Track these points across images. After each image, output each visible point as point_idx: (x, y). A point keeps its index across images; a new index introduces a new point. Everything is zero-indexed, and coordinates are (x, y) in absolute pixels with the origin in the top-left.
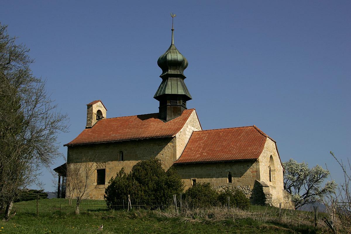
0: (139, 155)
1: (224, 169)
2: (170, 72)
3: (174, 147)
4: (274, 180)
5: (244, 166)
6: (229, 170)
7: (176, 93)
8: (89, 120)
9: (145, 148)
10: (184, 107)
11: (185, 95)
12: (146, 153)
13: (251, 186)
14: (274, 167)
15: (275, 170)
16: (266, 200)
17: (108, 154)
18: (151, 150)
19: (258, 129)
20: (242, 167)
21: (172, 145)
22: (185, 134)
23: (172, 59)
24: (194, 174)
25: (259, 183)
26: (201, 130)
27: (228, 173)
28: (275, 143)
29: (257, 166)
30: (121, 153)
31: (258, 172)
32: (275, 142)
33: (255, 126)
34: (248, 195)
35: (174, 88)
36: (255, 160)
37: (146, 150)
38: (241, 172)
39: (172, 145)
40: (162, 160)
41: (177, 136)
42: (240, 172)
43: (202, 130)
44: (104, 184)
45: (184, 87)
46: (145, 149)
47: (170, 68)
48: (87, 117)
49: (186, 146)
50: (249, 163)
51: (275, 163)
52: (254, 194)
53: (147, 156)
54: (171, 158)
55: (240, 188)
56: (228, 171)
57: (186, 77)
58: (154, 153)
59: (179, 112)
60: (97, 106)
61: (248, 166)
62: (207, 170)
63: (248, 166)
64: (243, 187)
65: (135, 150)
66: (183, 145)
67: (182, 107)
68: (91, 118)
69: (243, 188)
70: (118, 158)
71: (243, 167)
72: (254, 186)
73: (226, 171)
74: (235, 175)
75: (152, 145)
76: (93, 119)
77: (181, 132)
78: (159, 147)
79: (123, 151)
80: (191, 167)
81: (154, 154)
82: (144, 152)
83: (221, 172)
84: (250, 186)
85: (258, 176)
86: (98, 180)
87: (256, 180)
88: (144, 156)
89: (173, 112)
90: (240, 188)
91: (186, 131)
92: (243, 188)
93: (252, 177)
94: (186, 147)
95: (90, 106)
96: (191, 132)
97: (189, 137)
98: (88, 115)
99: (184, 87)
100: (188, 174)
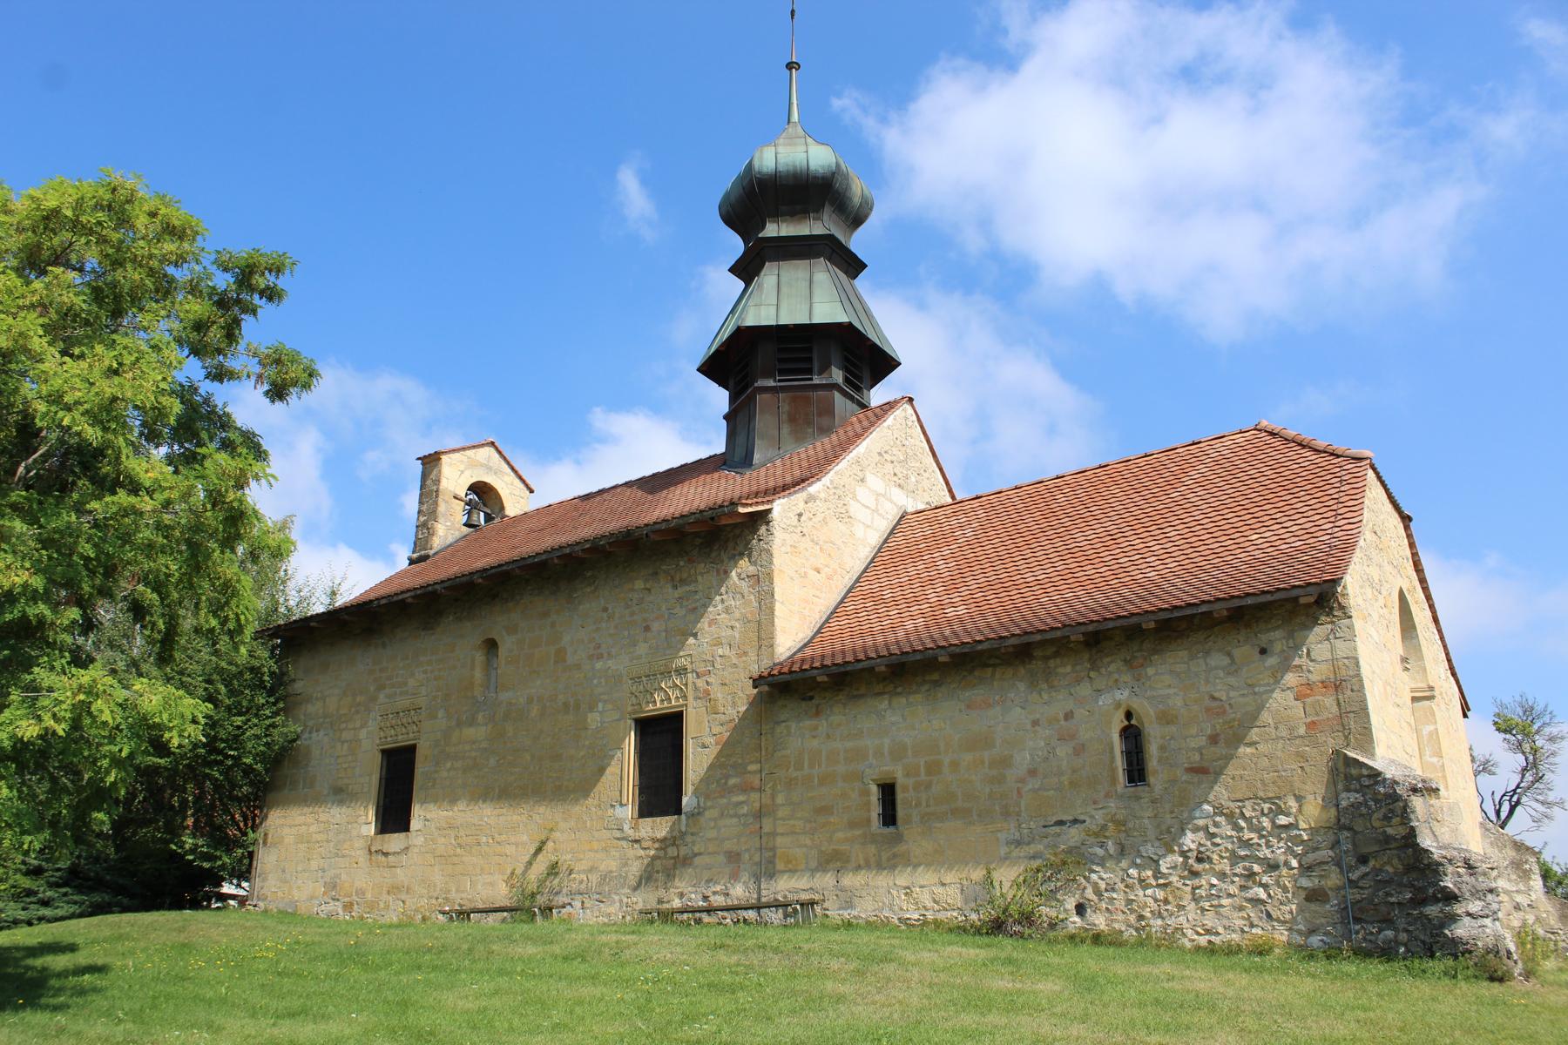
1: (1085, 690)
2: (771, 230)
3: (763, 583)
4: (1435, 760)
5: (1229, 654)
6: (1122, 695)
7: (802, 319)
10: (852, 398)
11: (850, 324)
13: (1299, 798)
14: (1425, 670)
15: (1431, 688)
16: (1459, 909)
18: (632, 614)
19: (1291, 433)
20: (1218, 660)
21: (752, 569)
22: (845, 517)
23: (780, 168)
24: (887, 741)
25: (1375, 775)
26: (950, 500)
27: (1120, 715)
28: (1407, 528)
29: (1338, 643)
31: (1345, 686)
32: (1406, 519)
33: (1264, 423)
34: (1284, 871)
35: (798, 297)
36: (1316, 601)
38: (1213, 698)
39: (752, 569)
41: (775, 514)
42: (1207, 702)
43: (953, 497)
44: (407, 829)
45: (851, 300)
47: (785, 214)
49: (852, 587)
50: (1269, 630)
51: (1424, 649)
52: (1338, 864)
54: (745, 654)
55: (1216, 825)
56: (1118, 705)
58: (647, 629)
59: (825, 421)
60: (473, 464)
61: (1263, 651)
62: (969, 707)
63: (1263, 651)
64: (1243, 815)
66: (829, 578)
67: (837, 395)
69: (1242, 823)
71: (1227, 661)
72: (1332, 800)
73: (1105, 701)
74: (1173, 729)
75: (639, 584)
76: (441, 520)
77: (811, 499)
78: (678, 593)
80: (862, 696)
83: (1069, 716)
84: (1292, 803)
85: (1352, 716)
87: (1337, 752)
88: (600, 657)
89: (792, 419)
90: (1216, 825)
91: (854, 498)
92: (1242, 823)
93: (1302, 731)
94: (849, 591)
95: (431, 462)
96: (892, 516)
97: (875, 539)
98: (421, 503)
99: (851, 300)
100: (849, 744)
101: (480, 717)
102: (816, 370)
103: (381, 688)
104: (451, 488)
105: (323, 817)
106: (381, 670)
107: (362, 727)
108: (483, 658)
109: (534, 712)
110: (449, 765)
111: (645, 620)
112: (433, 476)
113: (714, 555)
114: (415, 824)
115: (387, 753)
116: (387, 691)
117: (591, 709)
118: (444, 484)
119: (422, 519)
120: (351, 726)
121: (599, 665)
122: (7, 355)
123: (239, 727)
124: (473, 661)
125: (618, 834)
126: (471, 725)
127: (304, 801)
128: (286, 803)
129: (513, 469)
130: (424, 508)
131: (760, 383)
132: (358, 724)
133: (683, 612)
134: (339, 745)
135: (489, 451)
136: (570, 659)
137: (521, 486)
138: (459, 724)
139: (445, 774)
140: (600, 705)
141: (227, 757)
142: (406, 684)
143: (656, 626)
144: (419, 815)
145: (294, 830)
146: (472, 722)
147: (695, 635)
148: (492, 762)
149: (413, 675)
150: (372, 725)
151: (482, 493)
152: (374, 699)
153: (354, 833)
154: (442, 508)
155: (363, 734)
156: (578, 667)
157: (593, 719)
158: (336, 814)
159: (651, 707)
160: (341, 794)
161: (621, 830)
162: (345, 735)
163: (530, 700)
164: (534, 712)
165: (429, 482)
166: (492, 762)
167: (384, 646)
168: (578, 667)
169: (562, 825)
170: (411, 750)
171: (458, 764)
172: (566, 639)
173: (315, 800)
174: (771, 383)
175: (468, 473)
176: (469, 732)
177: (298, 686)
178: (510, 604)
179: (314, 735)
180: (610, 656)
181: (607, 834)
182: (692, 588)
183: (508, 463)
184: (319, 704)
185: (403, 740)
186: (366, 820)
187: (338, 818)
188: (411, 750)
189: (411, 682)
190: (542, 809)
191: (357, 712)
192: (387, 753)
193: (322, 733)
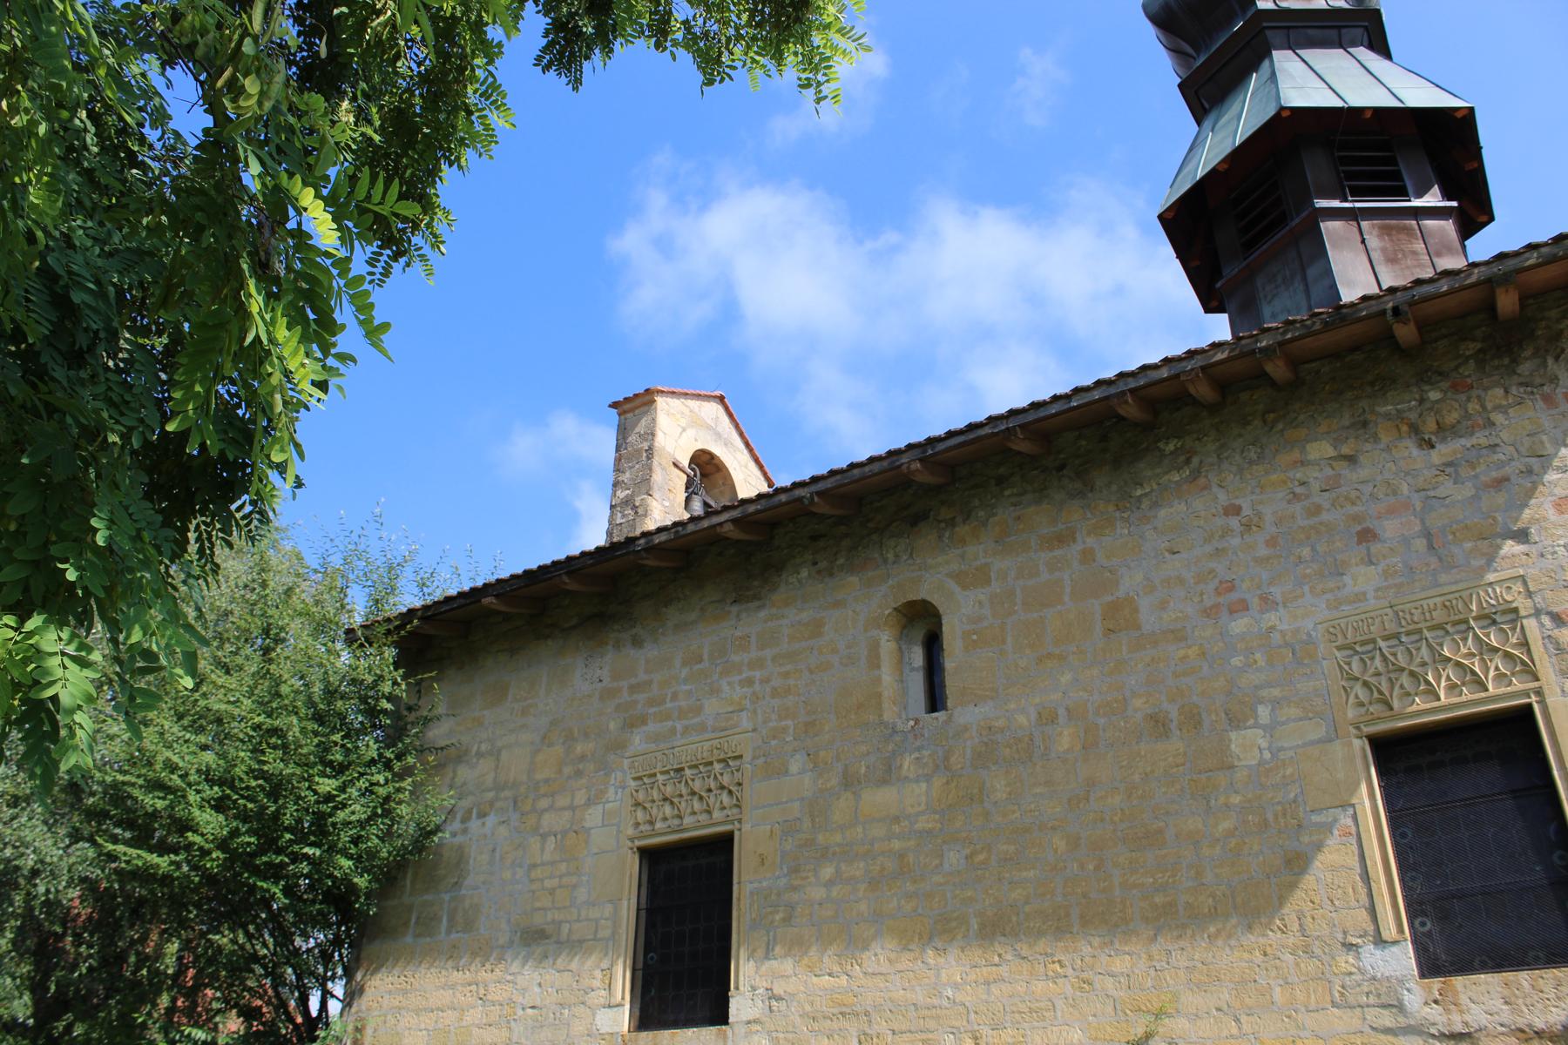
0: (1163, 605)
8: (628, 502)
9: (1237, 510)
12: (1260, 561)
17: (758, 664)
18: (1317, 510)
30: (919, 634)
37: (1247, 526)
40: (1537, 613)
46: (1234, 522)
48: (616, 485)
53: (1277, 592)
57: (644, 1034)
65: (1087, 556)
68: (644, 484)
70: (878, 680)
75: (1321, 449)
76: (656, 495)
78: (1436, 456)
79: (935, 599)
81: (1375, 548)
82: (1219, 552)
86: (1415, 908)
88: (1240, 607)
95: (633, 408)
98: (618, 469)
101: (907, 764)
102: (1410, 190)
103: (632, 723)
104: (670, 449)
105: (497, 993)
106: (633, 689)
107: (589, 803)
108: (892, 645)
109: (1065, 738)
110: (828, 872)
111: (1356, 518)
112: (641, 427)
113: (1525, 368)
114: (740, 1006)
115: (652, 857)
116: (651, 727)
117: (1236, 721)
118: (661, 440)
119: (621, 494)
120: (562, 801)
121: (1239, 625)
122: (5, 873)
123: (329, 798)
124: (874, 647)
125: (1387, 1019)
126: (884, 782)
127: (453, 954)
128: (413, 957)
129: (747, 445)
130: (626, 477)
131: (1322, 203)
132: (580, 798)
133: (1467, 491)
134: (534, 843)
135: (713, 410)
136: (1149, 619)
137: (758, 473)
138: (850, 782)
139: (818, 893)
140: (1264, 712)
141: (296, 858)
142: (698, 710)
143: (1390, 528)
144: (752, 981)
145: (427, 1020)
146: (887, 774)
147: (1522, 536)
148: (954, 858)
149: (715, 691)
150: (616, 798)
151: (706, 468)
152: (619, 746)
153: (578, 1028)
154: (657, 477)
155: (593, 817)
156: (1178, 635)
157: (1248, 745)
158: (527, 983)
159: (1420, 703)
160: (537, 940)
161: (1400, 1007)
162: (548, 821)
163: (1047, 718)
164: (1065, 738)
165: (632, 438)
166: (954, 858)
167: (637, 643)
168: (1178, 635)
169: (1191, 1000)
170: (722, 845)
171: (858, 869)
172: (1130, 582)
173: (485, 952)
174: (1336, 204)
175: (691, 432)
176: (880, 798)
177: (438, 734)
178: (962, 530)
179: (474, 824)
180: (1268, 603)
181: (1351, 1020)
182: (1480, 438)
183: (741, 435)
184: (485, 765)
185: (696, 825)
186: (604, 994)
187: (535, 996)
188: (722, 845)
189: (711, 706)
190: (1121, 964)
191: (579, 774)
192: (652, 857)
193: (491, 820)
